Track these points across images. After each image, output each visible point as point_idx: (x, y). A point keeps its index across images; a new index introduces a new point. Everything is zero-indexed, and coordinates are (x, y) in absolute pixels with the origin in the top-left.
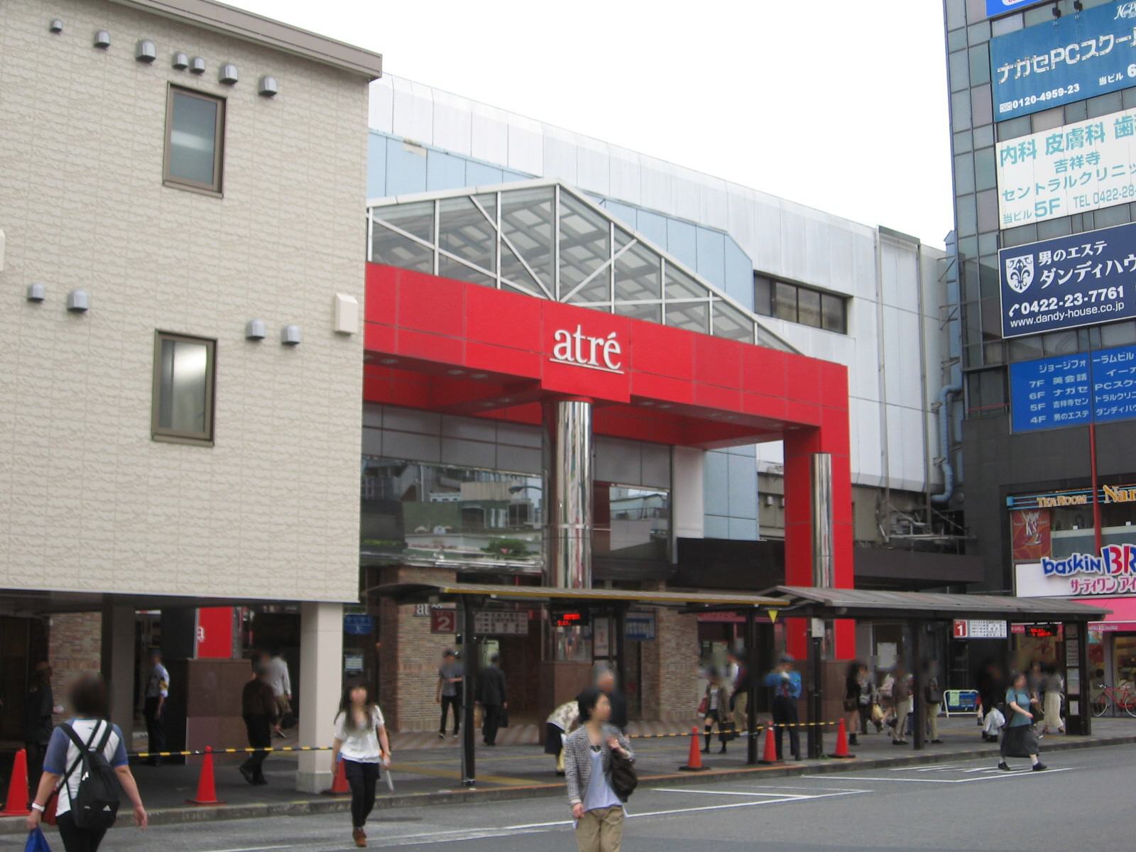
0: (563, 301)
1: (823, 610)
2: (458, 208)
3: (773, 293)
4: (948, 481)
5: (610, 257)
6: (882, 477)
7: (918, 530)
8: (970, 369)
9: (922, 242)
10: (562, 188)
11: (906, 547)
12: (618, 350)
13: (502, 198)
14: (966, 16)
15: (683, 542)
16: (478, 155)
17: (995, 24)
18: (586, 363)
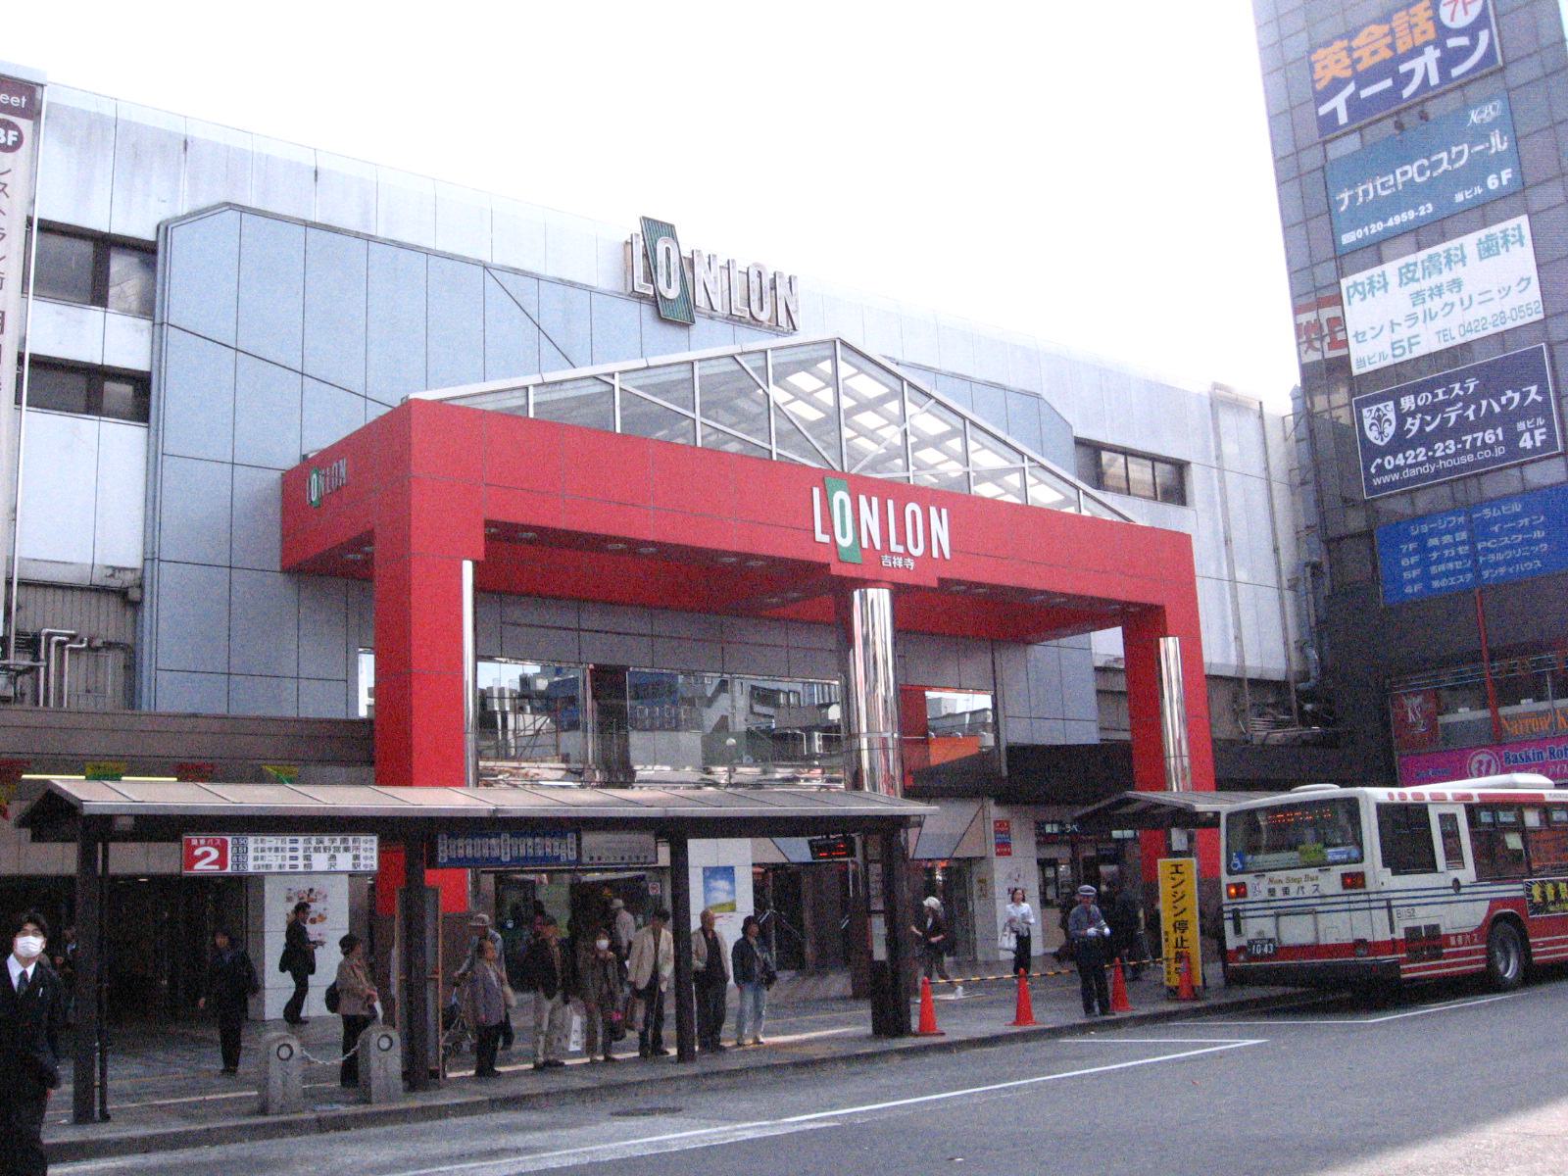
0: (853, 472)
3: (899, 456)
10: (843, 343)
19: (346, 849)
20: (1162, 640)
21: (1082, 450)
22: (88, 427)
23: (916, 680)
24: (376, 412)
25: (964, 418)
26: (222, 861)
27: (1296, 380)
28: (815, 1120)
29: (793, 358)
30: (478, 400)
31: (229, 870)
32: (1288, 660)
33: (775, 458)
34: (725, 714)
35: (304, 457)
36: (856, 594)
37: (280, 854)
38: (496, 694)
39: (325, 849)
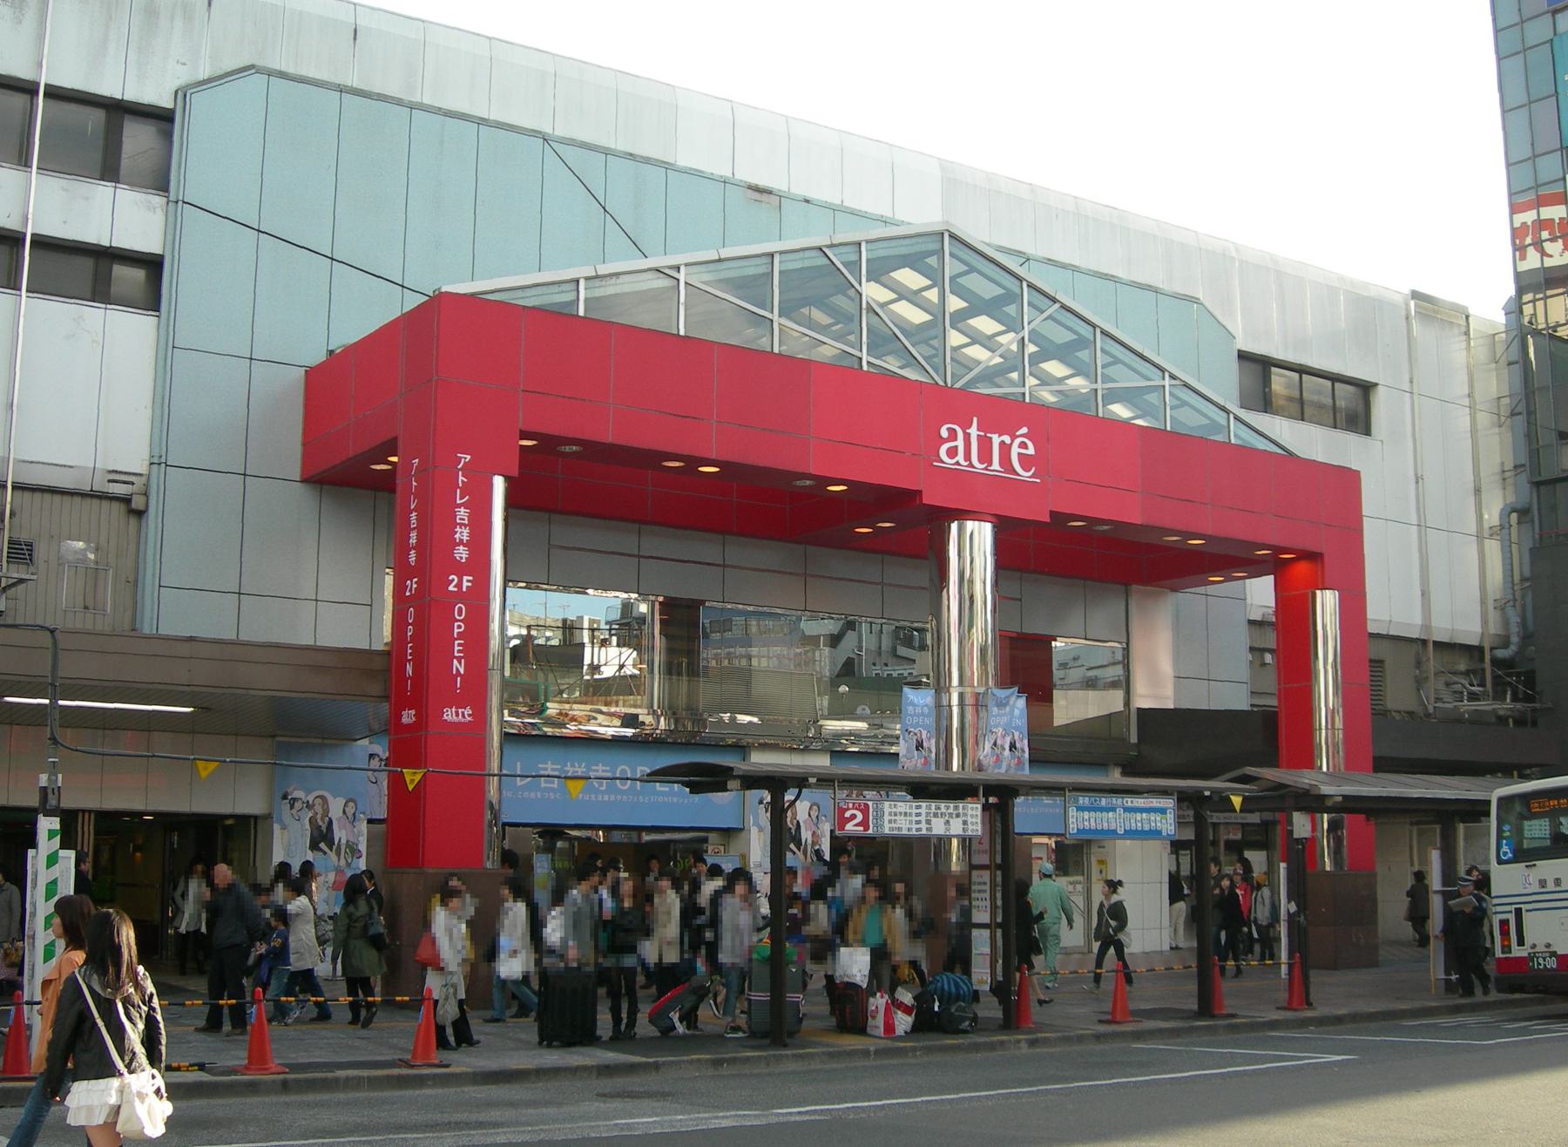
0: (957, 386)
1: (1312, 802)
2: (807, 264)
3: (1266, 380)
4: (1514, 629)
5: (1023, 328)
6: (1422, 625)
7: (1473, 697)
8: (1539, 479)
9: (1471, 311)
10: (953, 236)
11: (1478, 720)
12: (1031, 451)
13: (867, 250)
14: (1520, 10)
15: (1142, 712)
16: (850, 203)
17: (1558, 16)
18: (986, 469)
19: (958, 816)
20: (1318, 593)
21: (1247, 364)
22: (93, 315)
23: (1032, 627)
24: (413, 301)
25: (1094, 326)
26: (864, 823)
27: (1511, 291)
28: (807, 1112)
29: (896, 252)
30: (520, 294)
31: (870, 831)
32: (1485, 622)
33: (865, 367)
34: (852, 656)
35: (331, 352)
36: (954, 526)
37: (908, 818)
38: (586, 625)
39: (942, 814)
